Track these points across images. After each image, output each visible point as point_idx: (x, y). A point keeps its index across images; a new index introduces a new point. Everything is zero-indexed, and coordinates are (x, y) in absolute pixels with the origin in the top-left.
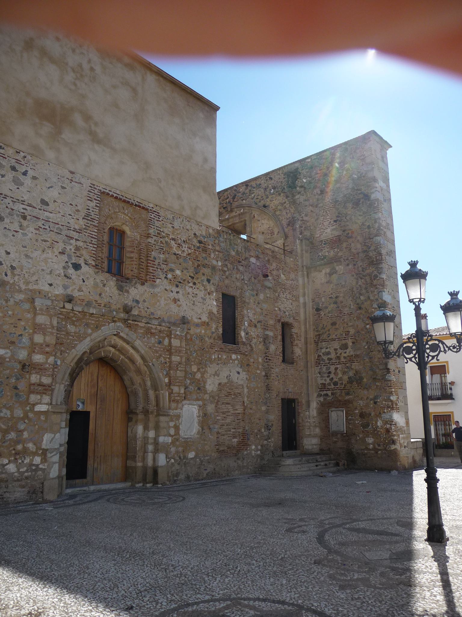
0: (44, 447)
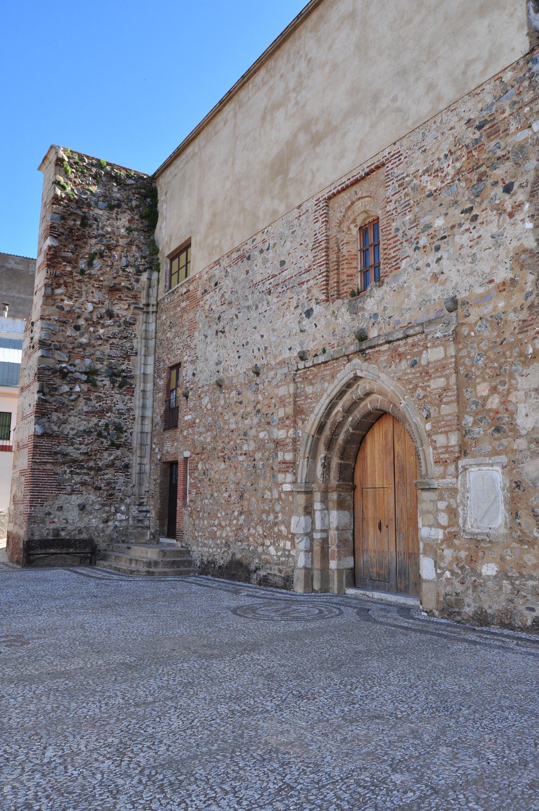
0: (292, 531)
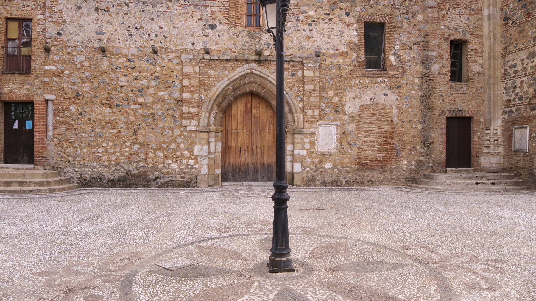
0: (195, 153)
